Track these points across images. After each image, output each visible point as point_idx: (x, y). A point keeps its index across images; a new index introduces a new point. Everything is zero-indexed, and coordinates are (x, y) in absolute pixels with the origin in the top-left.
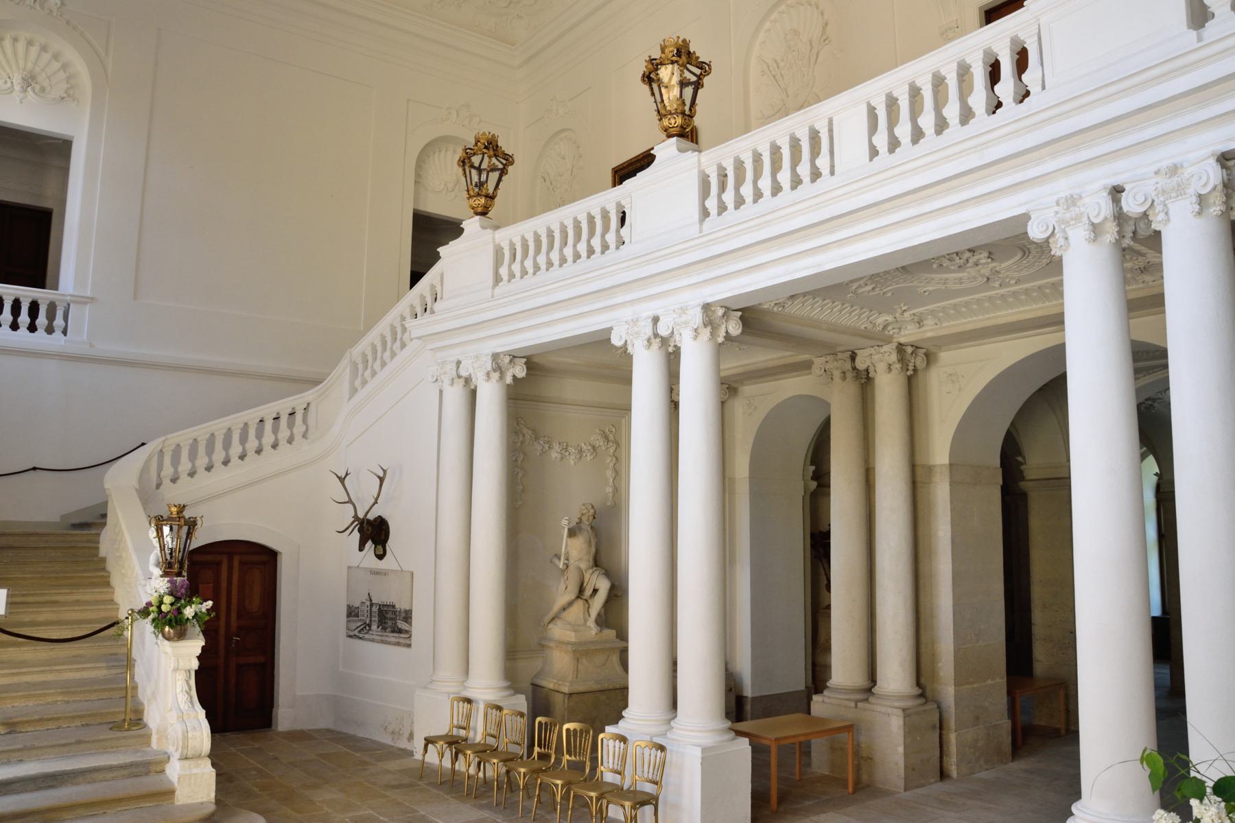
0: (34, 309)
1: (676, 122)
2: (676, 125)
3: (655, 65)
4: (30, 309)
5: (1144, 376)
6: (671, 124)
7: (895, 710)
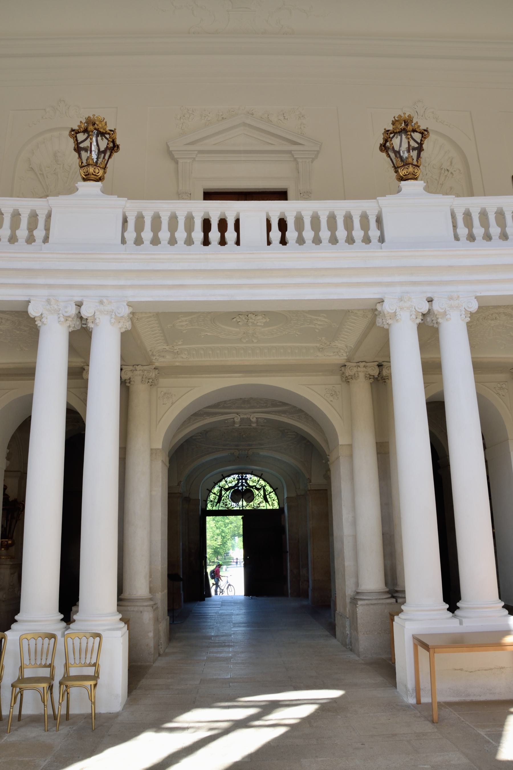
0: (223, 225)
1: (99, 173)
2: (98, 175)
3: (388, 136)
4: (219, 225)
5: (210, 418)
6: (95, 172)
7: (146, 608)
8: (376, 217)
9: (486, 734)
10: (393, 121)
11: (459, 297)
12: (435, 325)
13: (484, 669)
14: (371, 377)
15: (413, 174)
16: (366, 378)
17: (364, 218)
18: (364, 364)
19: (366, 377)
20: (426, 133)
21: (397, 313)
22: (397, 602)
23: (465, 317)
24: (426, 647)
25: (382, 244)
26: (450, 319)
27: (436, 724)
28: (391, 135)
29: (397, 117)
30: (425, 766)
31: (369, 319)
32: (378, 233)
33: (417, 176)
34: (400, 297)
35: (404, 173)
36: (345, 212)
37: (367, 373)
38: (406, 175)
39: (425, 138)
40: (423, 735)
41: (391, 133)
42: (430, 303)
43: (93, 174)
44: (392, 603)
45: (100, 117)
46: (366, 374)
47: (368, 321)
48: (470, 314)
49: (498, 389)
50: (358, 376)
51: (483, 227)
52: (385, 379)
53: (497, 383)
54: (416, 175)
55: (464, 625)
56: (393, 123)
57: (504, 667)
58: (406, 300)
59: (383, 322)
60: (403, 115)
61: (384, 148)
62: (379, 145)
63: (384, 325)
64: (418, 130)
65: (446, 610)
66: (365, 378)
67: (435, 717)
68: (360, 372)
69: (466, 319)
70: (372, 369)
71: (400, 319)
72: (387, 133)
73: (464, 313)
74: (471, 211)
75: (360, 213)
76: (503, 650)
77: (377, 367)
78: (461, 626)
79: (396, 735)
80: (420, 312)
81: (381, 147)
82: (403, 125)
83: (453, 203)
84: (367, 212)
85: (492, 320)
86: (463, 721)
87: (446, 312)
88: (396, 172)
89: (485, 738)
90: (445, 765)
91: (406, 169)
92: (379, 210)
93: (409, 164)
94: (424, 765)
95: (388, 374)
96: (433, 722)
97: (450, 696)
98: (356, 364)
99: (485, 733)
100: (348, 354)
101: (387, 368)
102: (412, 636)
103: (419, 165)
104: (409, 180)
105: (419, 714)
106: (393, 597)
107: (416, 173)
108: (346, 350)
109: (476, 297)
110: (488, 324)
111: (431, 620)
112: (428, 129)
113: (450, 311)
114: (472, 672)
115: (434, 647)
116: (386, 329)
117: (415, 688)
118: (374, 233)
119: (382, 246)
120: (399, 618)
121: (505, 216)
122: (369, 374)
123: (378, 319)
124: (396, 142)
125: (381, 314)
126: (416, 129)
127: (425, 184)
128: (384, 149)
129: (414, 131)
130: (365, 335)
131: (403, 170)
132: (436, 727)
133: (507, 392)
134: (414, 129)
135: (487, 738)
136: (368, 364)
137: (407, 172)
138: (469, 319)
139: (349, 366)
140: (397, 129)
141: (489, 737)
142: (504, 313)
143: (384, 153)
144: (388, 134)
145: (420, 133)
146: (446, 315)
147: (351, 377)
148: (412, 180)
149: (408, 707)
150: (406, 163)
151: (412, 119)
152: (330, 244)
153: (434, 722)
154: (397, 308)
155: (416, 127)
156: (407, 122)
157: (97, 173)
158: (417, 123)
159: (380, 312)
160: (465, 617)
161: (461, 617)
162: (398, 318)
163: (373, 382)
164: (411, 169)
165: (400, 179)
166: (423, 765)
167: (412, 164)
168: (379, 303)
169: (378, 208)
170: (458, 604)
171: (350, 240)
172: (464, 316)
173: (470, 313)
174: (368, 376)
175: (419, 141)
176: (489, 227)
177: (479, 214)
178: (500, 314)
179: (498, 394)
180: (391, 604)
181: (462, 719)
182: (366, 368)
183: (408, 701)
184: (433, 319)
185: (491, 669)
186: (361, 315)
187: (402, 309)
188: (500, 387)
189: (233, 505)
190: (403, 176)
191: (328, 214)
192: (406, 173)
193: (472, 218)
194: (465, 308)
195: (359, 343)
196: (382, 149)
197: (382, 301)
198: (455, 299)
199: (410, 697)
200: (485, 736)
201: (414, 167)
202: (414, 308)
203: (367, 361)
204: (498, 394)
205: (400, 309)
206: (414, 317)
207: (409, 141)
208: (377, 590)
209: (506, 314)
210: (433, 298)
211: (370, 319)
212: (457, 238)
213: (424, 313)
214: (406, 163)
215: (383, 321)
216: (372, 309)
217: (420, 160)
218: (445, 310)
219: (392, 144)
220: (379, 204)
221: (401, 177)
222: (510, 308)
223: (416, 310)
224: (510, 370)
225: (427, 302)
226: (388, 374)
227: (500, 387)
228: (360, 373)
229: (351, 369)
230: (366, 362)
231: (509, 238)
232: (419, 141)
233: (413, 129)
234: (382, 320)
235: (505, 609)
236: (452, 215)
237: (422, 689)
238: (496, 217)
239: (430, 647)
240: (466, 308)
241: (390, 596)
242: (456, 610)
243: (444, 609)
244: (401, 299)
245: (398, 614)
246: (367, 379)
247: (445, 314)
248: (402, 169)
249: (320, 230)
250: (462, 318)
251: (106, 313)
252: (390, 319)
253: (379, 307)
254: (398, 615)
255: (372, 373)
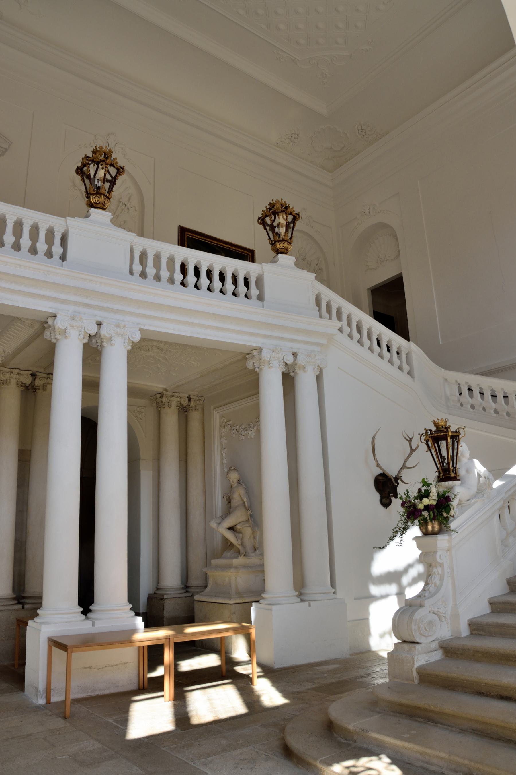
3: (86, 161)
8: (62, 235)
9: (114, 721)
10: (93, 149)
11: (125, 326)
12: (99, 348)
13: (111, 665)
14: (22, 384)
15: (103, 204)
16: (18, 385)
17: (50, 233)
18: (18, 371)
19: (18, 384)
20: (122, 170)
21: (67, 330)
22: (23, 607)
23: (127, 345)
24: (63, 647)
25: (64, 263)
26: (114, 344)
27: (67, 719)
28: (90, 162)
29: (98, 148)
30: (64, 757)
31: (35, 329)
32: (61, 251)
33: (106, 207)
34: (72, 316)
35: (95, 201)
36: (33, 222)
37: (19, 380)
38: (96, 203)
39: (120, 175)
40: (58, 731)
41: (90, 160)
42: (98, 326)
44: (18, 609)
46: (18, 381)
47: (34, 331)
48: (132, 343)
49: (137, 413)
50: (10, 382)
51: (155, 268)
52: (35, 389)
53: (137, 407)
54: (105, 206)
55: (96, 626)
56: (94, 152)
57: (128, 663)
58: (77, 320)
59: (51, 336)
60: (104, 148)
61: (80, 171)
62: (76, 167)
63: (52, 339)
64: (115, 166)
65: (80, 613)
66: (17, 385)
67: (68, 713)
68: (13, 378)
69: (128, 347)
70: (25, 377)
71: (69, 336)
72: (87, 160)
73: (127, 341)
74: (147, 251)
75: (47, 227)
76: (132, 646)
77: (30, 377)
78: (94, 627)
79: (31, 735)
80: (87, 333)
81: (78, 170)
82: (103, 156)
83: (134, 240)
84: (54, 227)
85: (145, 350)
86: (92, 714)
87: (111, 338)
88: (88, 197)
89: (114, 724)
90: (81, 752)
91: (98, 198)
92: (66, 229)
93: (102, 194)
94: (63, 756)
95: (40, 385)
96: (65, 718)
97: (78, 693)
98: (9, 370)
99: (113, 721)
100: (3, 358)
101: (40, 378)
102: (47, 638)
103: (110, 197)
104: (99, 209)
105: (50, 713)
106: (19, 603)
107: (106, 204)
108: (3, 354)
109: (140, 330)
110: (141, 353)
111: (66, 622)
112: (124, 168)
113: (115, 337)
114: (100, 669)
115: (72, 647)
116: (53, 343)
117: (46, 689)
118: (57, 249)
119: (63, 264)
120: (34, 622)
121: (175, 263)
122: (21, 382)
123: (46, 332)
124: (92, 169)
125: (50, 327)
126: (114, 165)
127: (112, 217)
128: (80, 172)
129: (112, 165)
130: (27, 343)
131: (94, 198)
132: (68, 722)
133: (144, 417)
134: (112, 164)
135: (115, 724)
136: (22, 372)
137: (98, 201)
138: (131, 348)
139: (2, 370)
140: (97, 159)
141: (117, 723)
142: (157, 346)
143: (79, 176)
144: (88, 160)
145: (116, 168)
146: (111, 341)
147: (3, 382)
148: (101, 210)
149: (38, 708)
150: (98, 191)
151: (111, 154)
152: (13, 250)
153: (66, 718)
154: (68, 326)
155: (114, 162)
156: (107, 155)
158: (116, 159)
159: (50, 326)
160: (97, 619)
161: (93, 619)
162: (67, 335)
163: (24, 390)
164: (102, 199)
165: (89, 205)
166: (61, 756)
167: (104, 195)
168: (51, 317)
169: (65, 227)
170: (91, 607)
171: (33, 251)
172: (127, 344)
173: (132, 342)
174: (20, 383)
175: (113, 176)
176: (161, 270)
177: (154, 256)
178: (153, 347)
179: (136, 417)
180: (17, 610)
181: (91, 712)
182: (19, 375)
183: (37, 702)
184: (98, 341)
185: (116, 665)
186: (28, 325)
187: (72, 327)
188: (139, 411)
190: (93, 203)
191: (15, 220)
192: (97, 201)
193: (161, 260)
194: (129, 337)
195: (18, 351)
196: (79, 172)
197: (55, 316)
198: (122, 328)
199: (40, 698)
200: (114, 723)
201: (105, 198)
202: (83, 328)
203: (22, 369)
204: (136, 417)
205: (70, 327)
206: (82, 337)
207: (106, 173)
208: (4, 596)
209: (158, 348)
210: (103, 323)
211: (36, 330)
212: (131, 273)
213: (92, 335)
214: (98, 191)
215: (52, 334)
216: (41, 321)
217: (112, 193)
218: (111, 336)
219: (89, 171)
220: (68, 223)
221: (91, 203)
222: (163, 343)
223: (85, 331)
224: (151, 397)
225: (96, 325)
226: (40, 385)
227: (139, 411)
228: (12, 380)
229: (4, 374)
230: (20, 370)
231: (189, 286)
232: (113, 176)
233: (111, 163)
234: (51, 333)
235: (132, 611)
236: (131, 251)
237: (53, 689)
238: (167, 262)
239: (68, 647)
240: (130, 338)
241: (16, 602)
242: (88, 613)
243: (79, 612)
244: (73, 318)
245: (32, 618)
246: (18, 387)
247: (110, 339)
248: (94, 197)
249: (53, 245)
250: (125, 346)
252: (60, 334)
253: (50, 321)
254: (33, 619)
255: (24, 381)
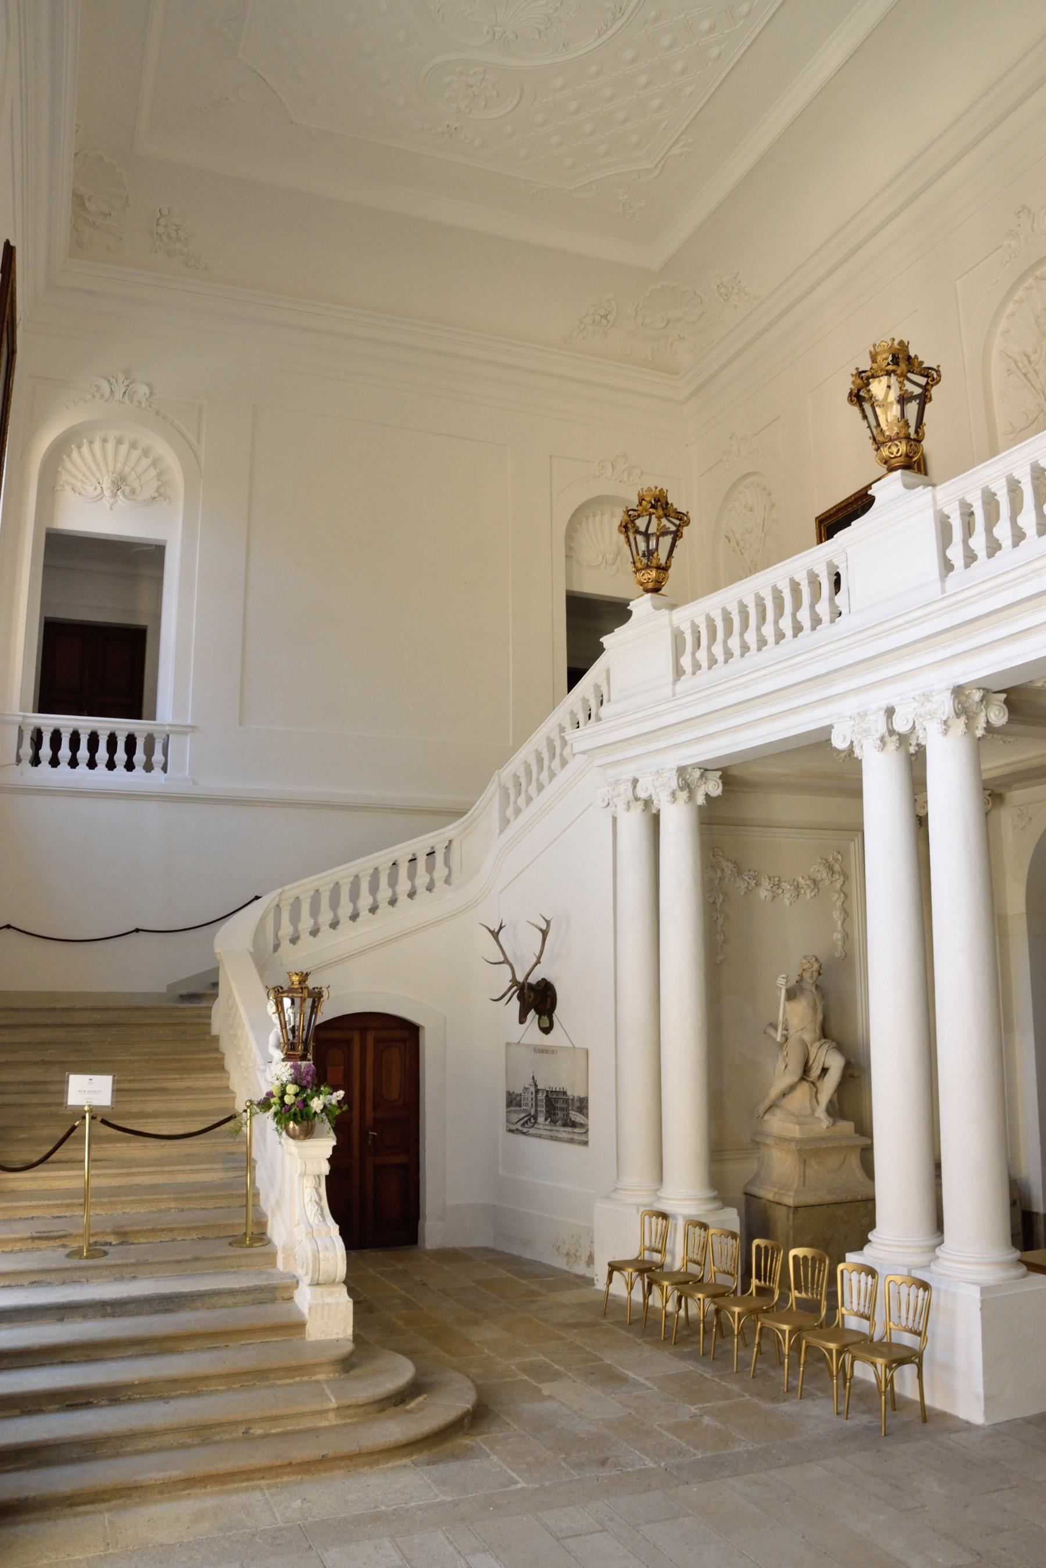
1: (898, 451)
6: (892, 454)
43: (892, 458)
45: (883, 343)
60: (654, 489)
157: (897, 453)
189: (585, 1258)
251: (929, 717)
